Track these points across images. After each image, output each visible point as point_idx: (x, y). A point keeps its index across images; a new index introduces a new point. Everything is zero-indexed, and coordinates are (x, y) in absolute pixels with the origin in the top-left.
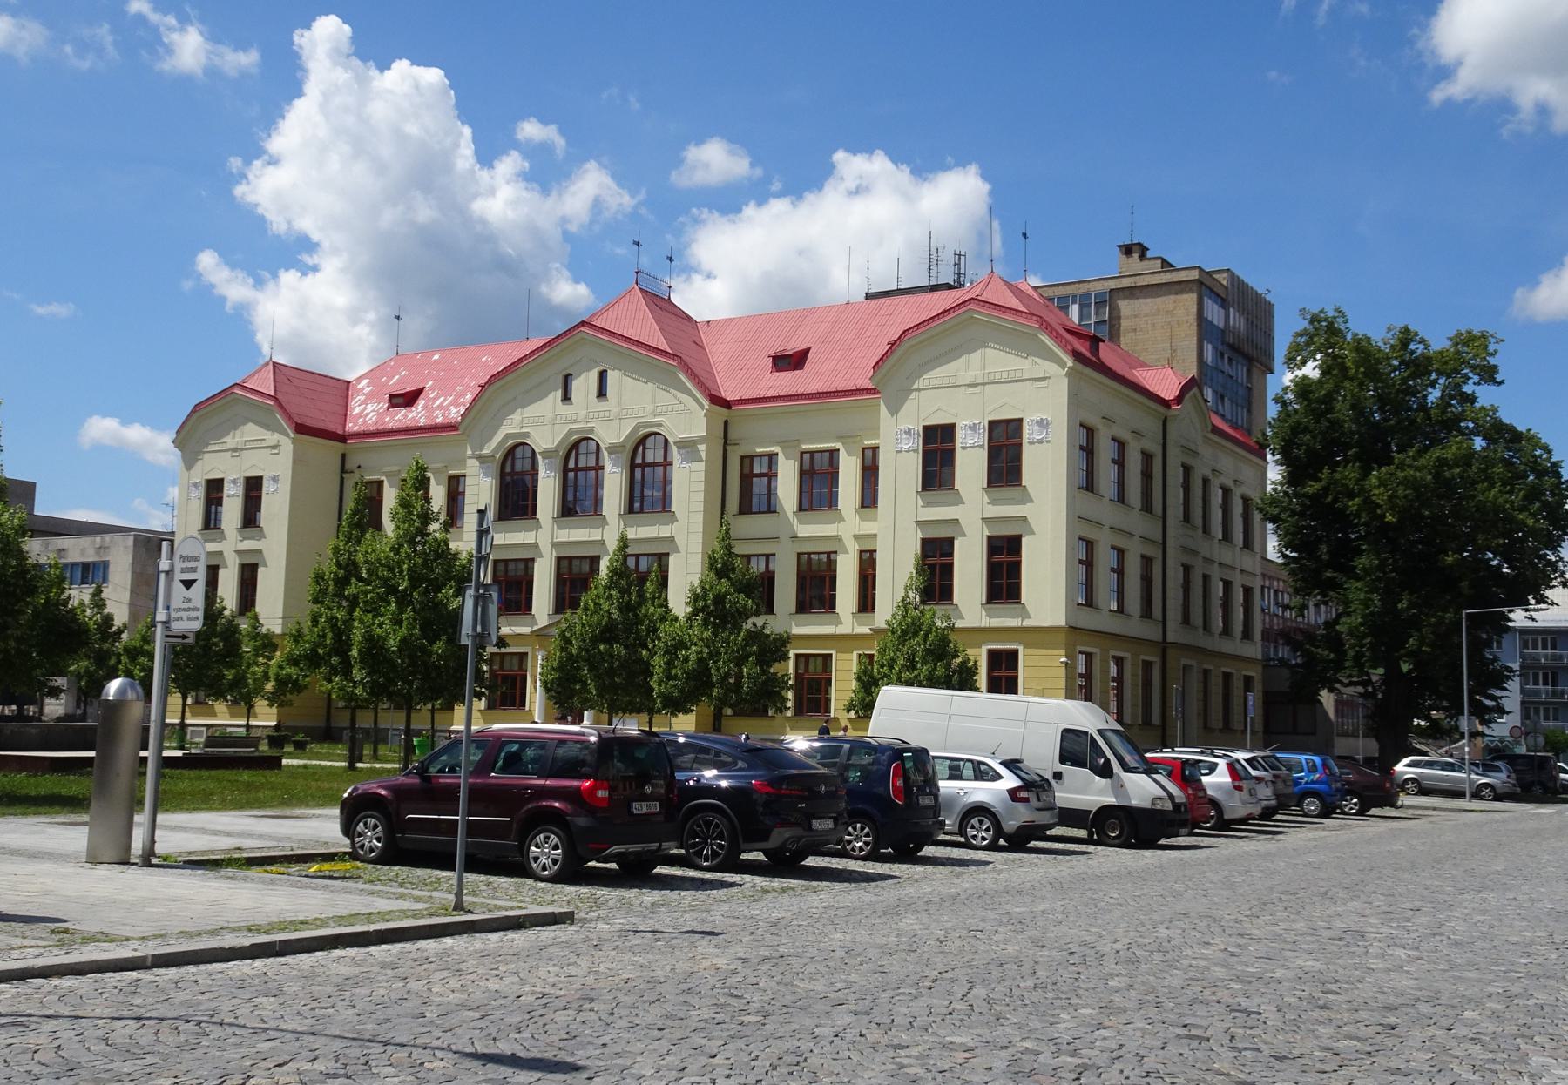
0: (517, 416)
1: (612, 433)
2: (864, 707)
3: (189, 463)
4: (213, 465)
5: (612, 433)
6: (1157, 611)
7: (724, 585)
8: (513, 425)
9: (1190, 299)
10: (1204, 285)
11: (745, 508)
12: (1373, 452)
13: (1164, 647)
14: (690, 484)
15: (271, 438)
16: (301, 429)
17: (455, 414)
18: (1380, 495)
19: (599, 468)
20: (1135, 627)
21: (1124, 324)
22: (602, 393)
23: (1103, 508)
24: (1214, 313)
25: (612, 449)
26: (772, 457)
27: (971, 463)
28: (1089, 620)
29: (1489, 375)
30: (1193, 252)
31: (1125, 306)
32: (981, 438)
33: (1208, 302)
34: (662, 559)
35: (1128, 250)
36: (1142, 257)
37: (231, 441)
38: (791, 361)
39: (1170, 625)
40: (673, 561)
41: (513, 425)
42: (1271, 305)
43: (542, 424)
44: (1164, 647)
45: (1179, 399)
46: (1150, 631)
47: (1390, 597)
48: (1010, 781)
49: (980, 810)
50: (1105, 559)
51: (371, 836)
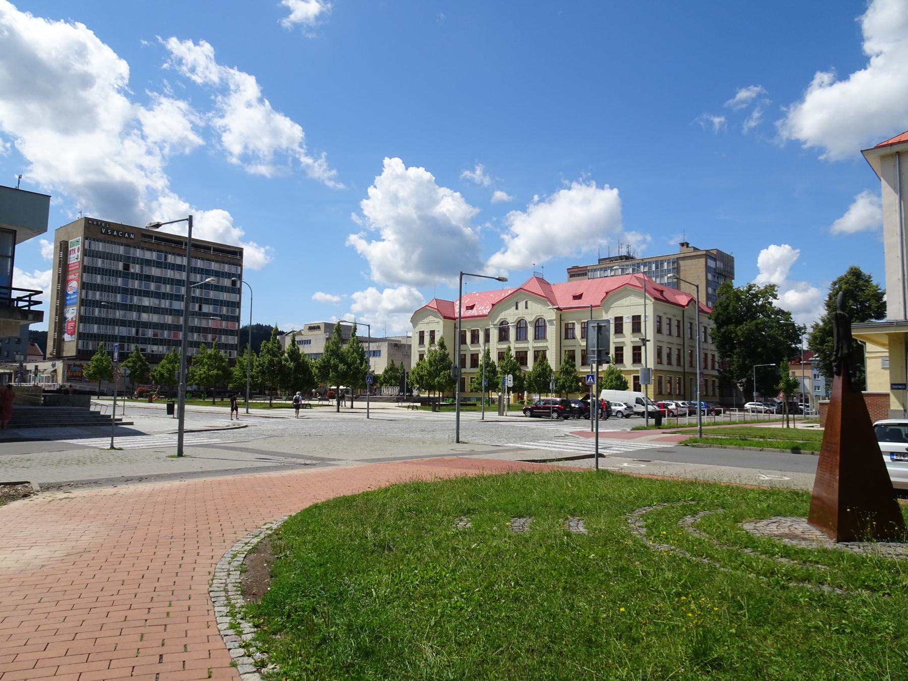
0: (503, 313)
1: (530, 318)
2: (599, 392)
3: (414, 326)
4: (421, 327)
5: (530, 318)
6: (682, 364)
7: (568, 366)
8: (502, 316)
9: (703, 260)
10: (708, 255)
11: (567, 338)
12: (739, 321)
13: (684, 373)
14: (551, 332)
15: (437, 320)
16: (445, 317)
17: (486, 312)
18: (739, 333)
19: (526, 327)
20: (675, 368)
21: (682, 268)
22: (526, 308)
23: (664, 337)
24: (712, 264)
25: (530, 322)
26: (573, 324)
27: (627, 327)
28: (660, 367)
29: (775, 297)
30: (705, 245)
31: (681, 263)
32: (630, 320)
33: (709, 261)
34: (544, 352)
35: (682, 245)
36: (687, 247)
37: (426, 321)
38: (578, 297)
39: (686, 367)
40: (548, 353)
41: (502, 316)
42: (733, 258)
43: (510, 316)
44: (684, 373)
45: (687, 305)
46: (680, 369)
47: (744, 360)
48: (625, 406)
49: (619, 411)
50: (665, 352)
51: (528, 413)
